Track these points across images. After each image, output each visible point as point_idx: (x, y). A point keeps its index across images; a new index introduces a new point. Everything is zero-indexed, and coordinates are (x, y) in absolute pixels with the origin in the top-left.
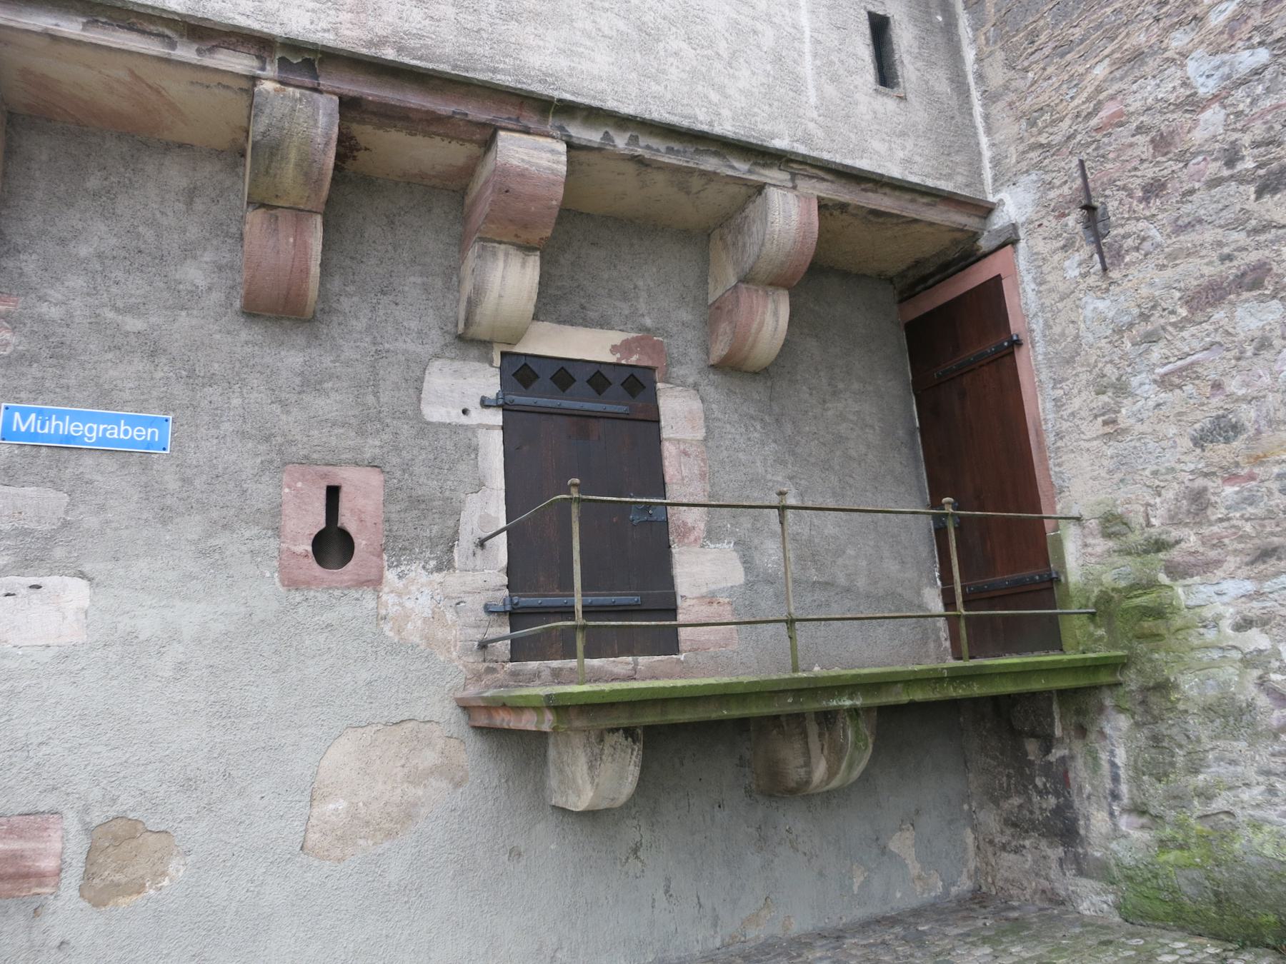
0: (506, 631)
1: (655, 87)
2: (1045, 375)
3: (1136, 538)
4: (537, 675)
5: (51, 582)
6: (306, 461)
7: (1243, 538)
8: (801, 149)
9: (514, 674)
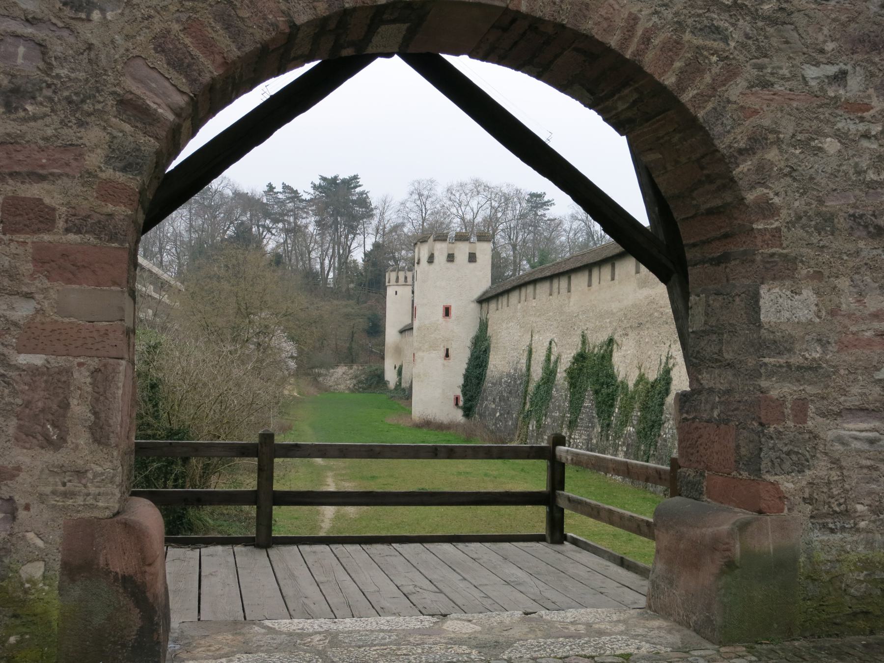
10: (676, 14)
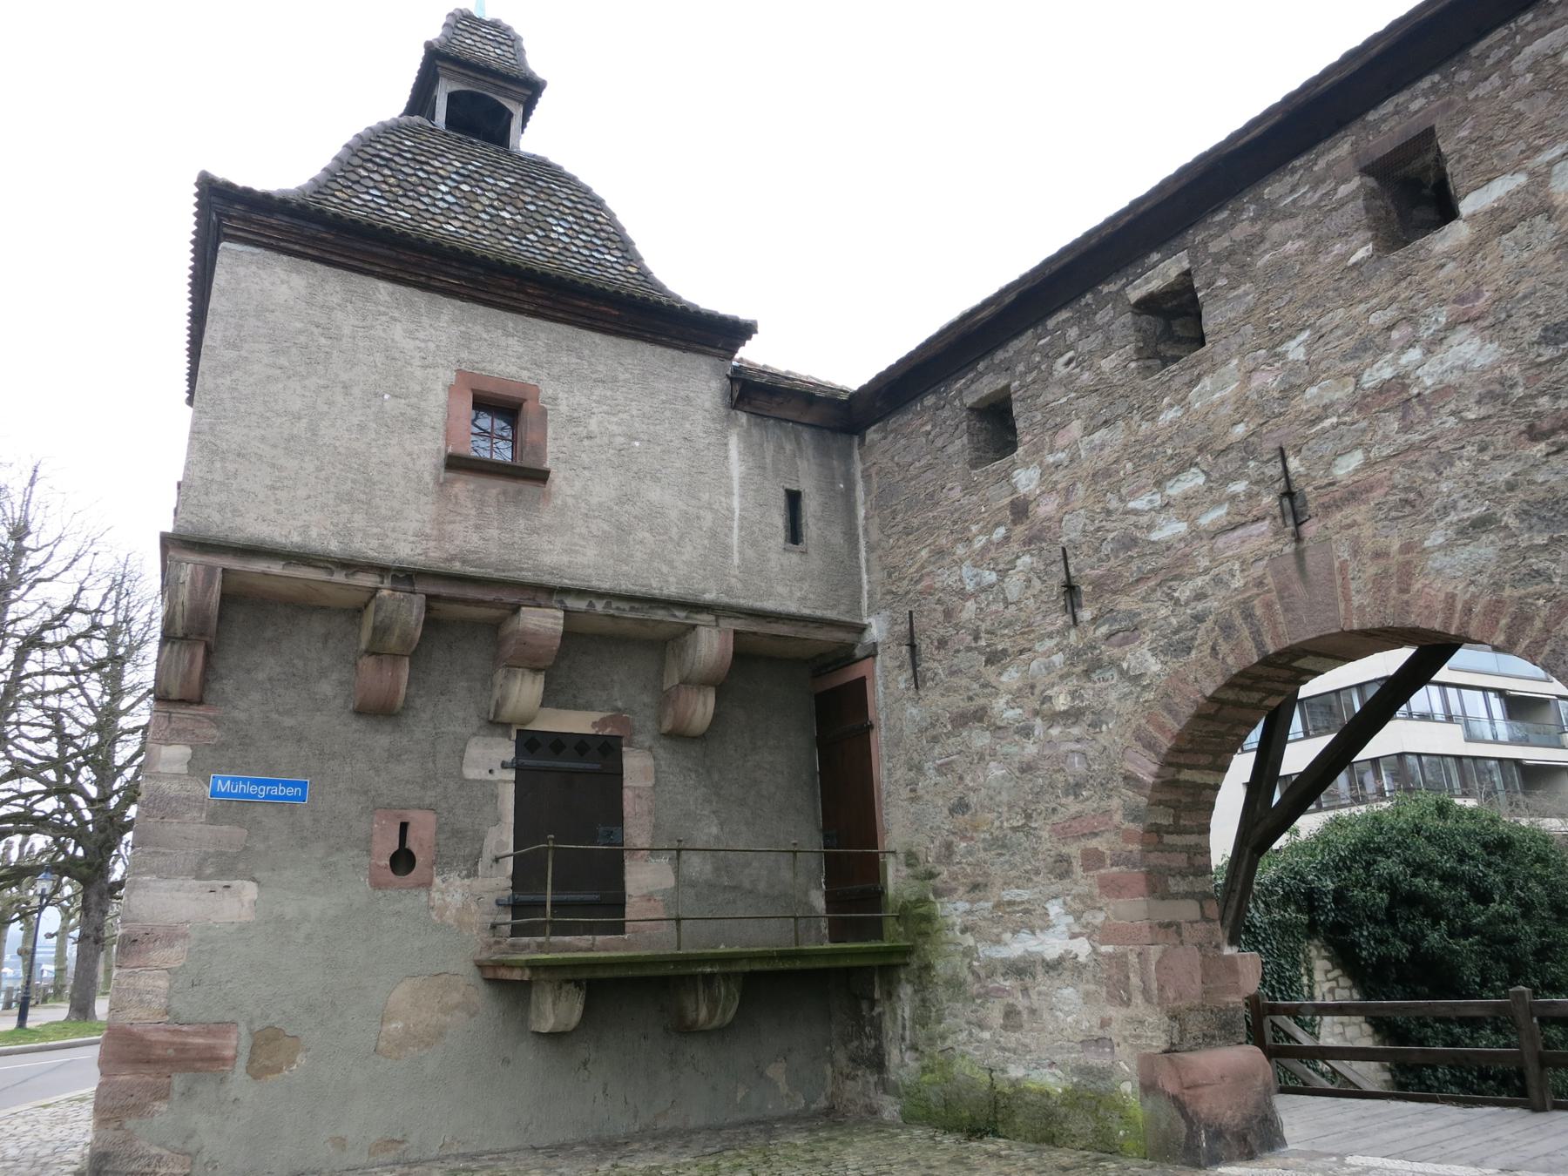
0: (509, 918)
1: (625, 568)
2: (884, 751)
3: (921, 869)
4: (527, 946)
5: (236, 883)
6: (389, 807)
7: (966, 876)
8: (725, 599)
9: (513, 945)
10: (1491, 576)
